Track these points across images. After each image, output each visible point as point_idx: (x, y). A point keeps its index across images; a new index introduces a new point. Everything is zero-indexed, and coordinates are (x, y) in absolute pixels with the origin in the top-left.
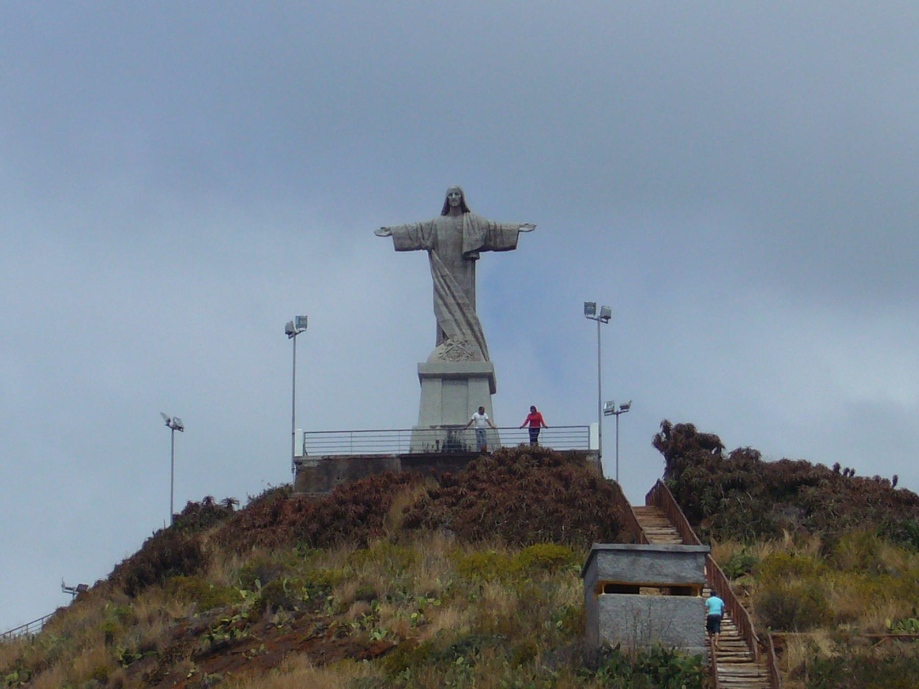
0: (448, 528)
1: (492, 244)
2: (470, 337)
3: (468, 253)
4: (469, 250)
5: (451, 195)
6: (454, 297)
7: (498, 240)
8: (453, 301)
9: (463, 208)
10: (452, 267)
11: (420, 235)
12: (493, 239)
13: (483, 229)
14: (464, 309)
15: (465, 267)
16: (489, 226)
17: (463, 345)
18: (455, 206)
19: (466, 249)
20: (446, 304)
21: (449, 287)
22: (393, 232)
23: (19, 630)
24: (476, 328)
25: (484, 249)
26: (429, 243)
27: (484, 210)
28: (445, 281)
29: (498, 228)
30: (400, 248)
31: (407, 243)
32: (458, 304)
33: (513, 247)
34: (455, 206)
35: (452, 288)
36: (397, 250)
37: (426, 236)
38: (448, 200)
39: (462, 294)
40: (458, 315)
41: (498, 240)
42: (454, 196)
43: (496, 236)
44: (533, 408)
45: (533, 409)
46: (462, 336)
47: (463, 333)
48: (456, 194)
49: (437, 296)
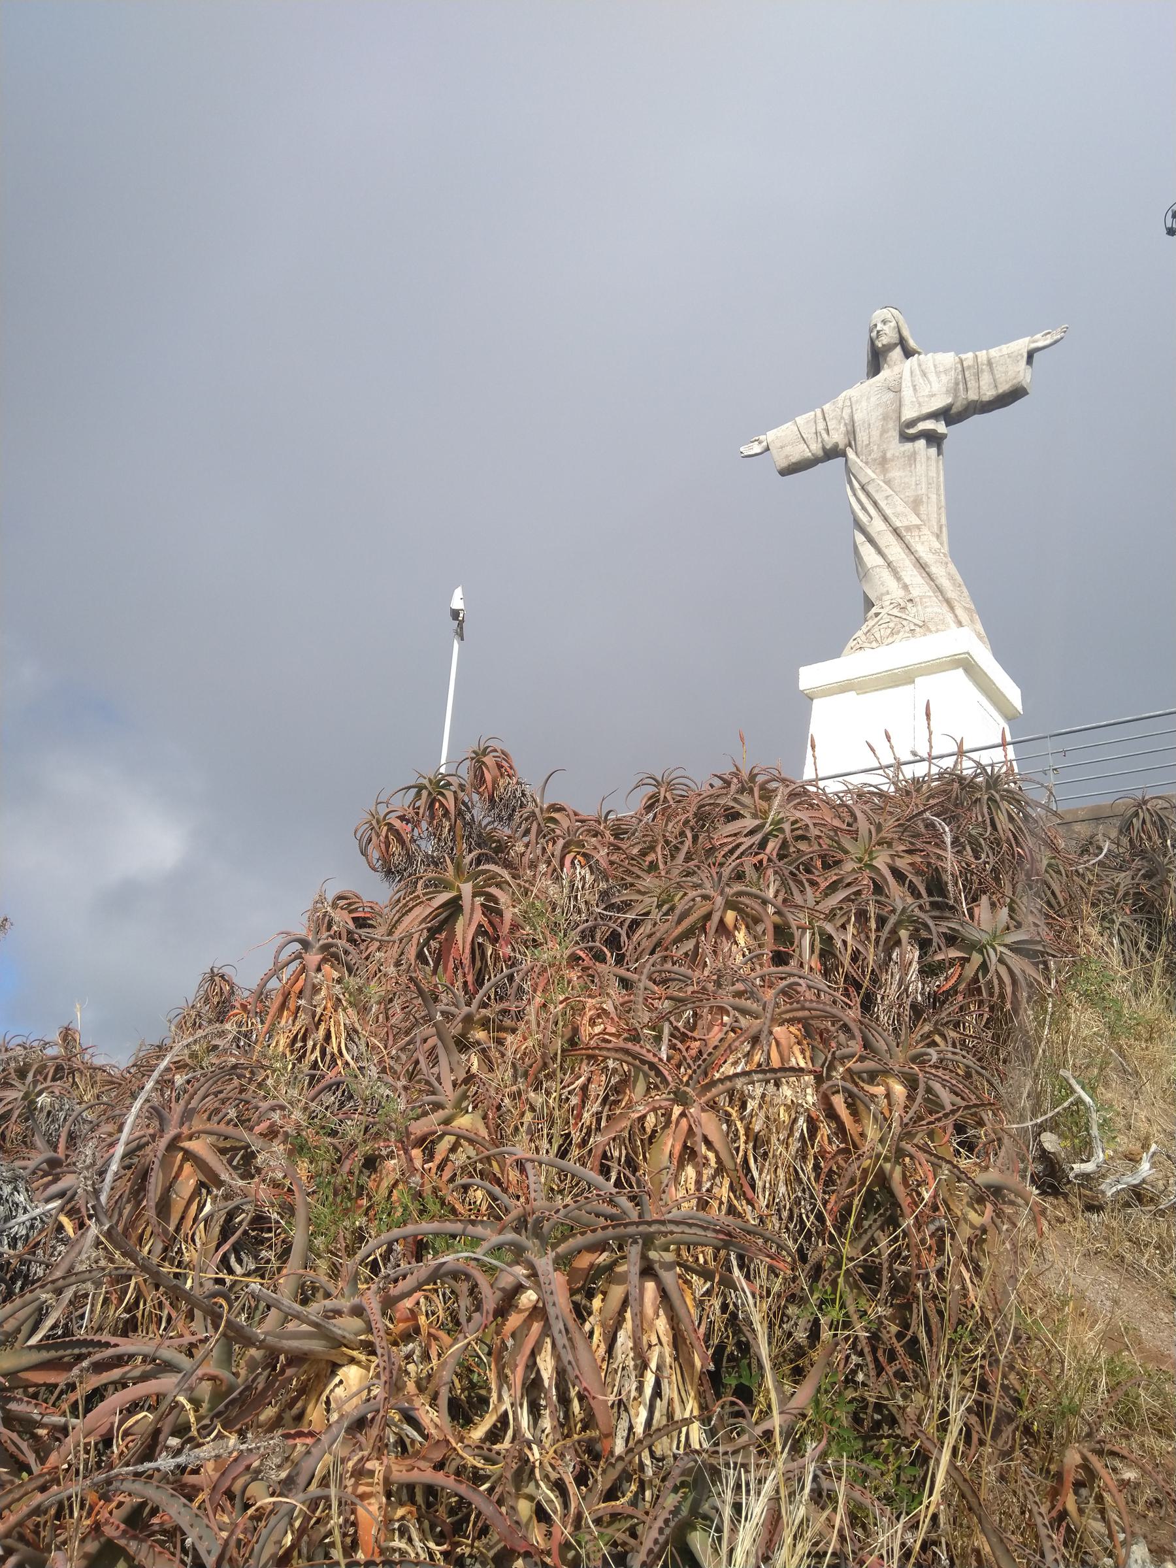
1: (973, 396)
3: (912, 423)
6: (886, 519)
11: (821, 426)
13: (946, 372)
14: (908, 538)
19: (908, 414)
32: (896, 531)
35: (882, 504)
39: (901, 507)
46: (901, 593)
47: (906, 587)
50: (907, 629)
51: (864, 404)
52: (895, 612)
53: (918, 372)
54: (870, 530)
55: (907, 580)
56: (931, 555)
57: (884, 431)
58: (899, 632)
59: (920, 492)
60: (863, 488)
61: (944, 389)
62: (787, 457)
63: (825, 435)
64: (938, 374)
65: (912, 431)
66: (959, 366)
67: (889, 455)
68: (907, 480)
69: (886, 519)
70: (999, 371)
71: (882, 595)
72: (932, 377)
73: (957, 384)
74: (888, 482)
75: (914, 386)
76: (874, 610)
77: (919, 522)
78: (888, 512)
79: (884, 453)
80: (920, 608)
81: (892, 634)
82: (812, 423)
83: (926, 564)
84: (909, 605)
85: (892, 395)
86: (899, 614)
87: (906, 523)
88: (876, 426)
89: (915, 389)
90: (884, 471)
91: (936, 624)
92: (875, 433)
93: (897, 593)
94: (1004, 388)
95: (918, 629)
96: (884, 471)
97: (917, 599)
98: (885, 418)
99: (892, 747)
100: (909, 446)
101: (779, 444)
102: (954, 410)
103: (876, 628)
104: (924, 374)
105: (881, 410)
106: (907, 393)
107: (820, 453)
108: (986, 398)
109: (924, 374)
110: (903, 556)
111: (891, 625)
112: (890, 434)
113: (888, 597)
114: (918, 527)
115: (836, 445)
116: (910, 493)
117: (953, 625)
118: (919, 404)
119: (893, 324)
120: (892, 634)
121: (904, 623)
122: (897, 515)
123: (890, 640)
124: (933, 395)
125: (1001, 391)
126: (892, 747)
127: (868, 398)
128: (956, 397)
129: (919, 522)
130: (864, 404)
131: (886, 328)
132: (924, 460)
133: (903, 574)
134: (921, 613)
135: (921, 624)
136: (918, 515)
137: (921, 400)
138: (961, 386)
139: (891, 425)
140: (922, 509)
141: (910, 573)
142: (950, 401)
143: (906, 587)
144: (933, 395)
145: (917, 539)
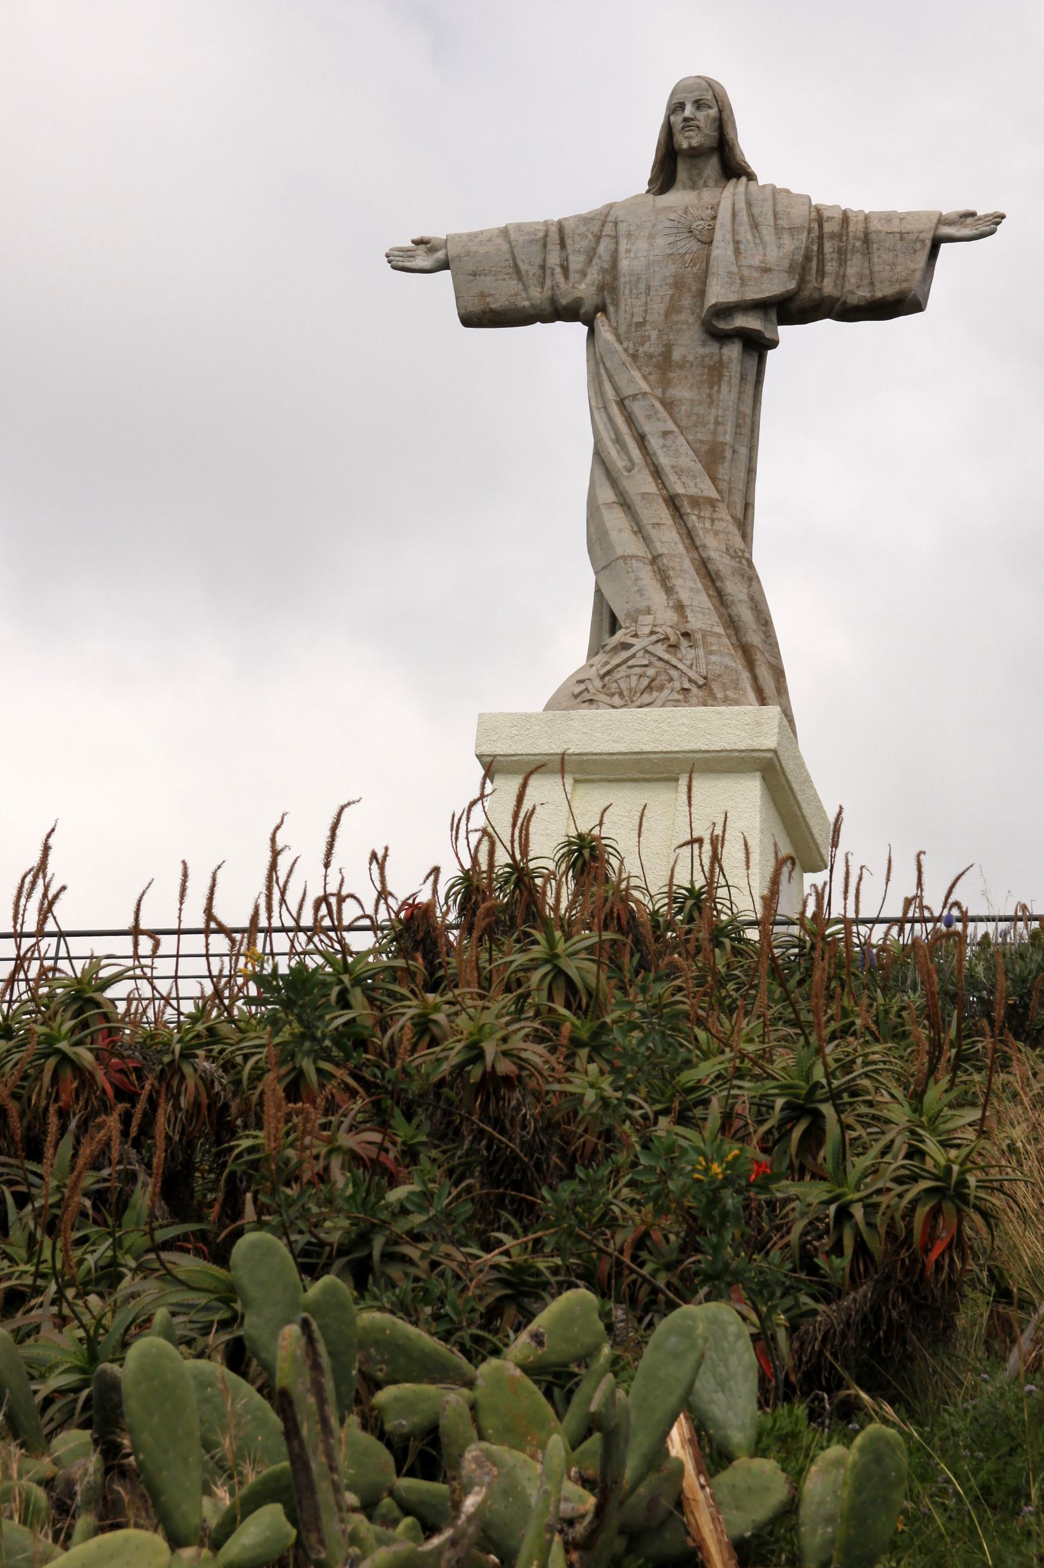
0: (696, 1274)
1: (829, 287)
2: (703, 616)
3: (725, 311)
4: (732, 298)
5: (681, 106)
6: (657, 473)
7: (859, 275)
8: (651, 487)
9: (733, 168)
10: (664, 365)
11: (554, 258)
12: (830, 267)
13: (792, 230)
14: (693, 519)
15: (716, 372)
16: (820, 220)
17: (674, 647)
18: (699, 147)
19: (718, 293)
20: (625, 504)
21: (641, 440)
22: (453, 250)
23: (990, 927)
24: (734, 588)
25: (794, 309)
26: (584, 289)
27: (807, 155)
28: (630, 420)
29: (856, 228)
30: (478, 317)
31: (504, 292)
32: (673, 502)
33: (902, 303)
34: (699, 147)
35: (655, 443)
36: (469, 320)
37: (576, 262)
38: (668, 132)
39: (687, 459)
40: (668, 539)
41: (859, 275)
42: (689, 111)
43: (842, 255)
44: (998, 218)
45: (998, 218)
46: (671, 616)
47: (680, 608)
48: (698, 104)
49: (600, 475)
50: (677, 685)
51: (642, 245)
52: (660, 650)
53: (743, 217)
54: (626, 483)
55: (684, 596)
56: (726, 559)
57: (673, 309)
58: (661, 688)
59: (720, 439)
60: (621, 403)
61: (786, 264)
62: (482, 295)
63: (559, 277)
64: (778, 229)
65: (722, 325)
66: (815, 225)
67: (676, 355)
68: (702, 410)
69: (657, 473)
70: (881, 258)
71: (638, 611)
72: (768, 233)
73: (807, 258)
74: (669, 405)
75: (737, 243)
76: (619, 636)
77: (714, 494)
78: (664, 461)
79: (668, 348)
80: (701, 652)
81: (649, 688)
82: (538, 247)
83: (717, 573)
84: (684, 643)
85: (694, 245)
86: (666, 656)
87: (693, 491)
88: (662, 294)
89: (737, 252)
90: (665, 383)
91: (725, 688)
92: (658, 307)
93: (666, 617)
94: (884, 290)
95: (694, 690)
96: (665, 383)
97: (698, 636)
98: (678, 284)
99: (180, 910)
100: (713, 348)
101: (471, 267)
102: (797, 304)
103: (623, 671)
104: (755, 225)
105: (672, 269)
106: (722, 251)
107: (547, 306)
108: (853, 300)
109: (755, 225)
110: (681, 549)
111: (651, 672)
112: (683, 317)
113: (649, 619)
114: (712, 503)
115: (578, 302)
116: (703, 435)
117: (751, 695)
118: (742, 279)
119: (713, 112)
120: (649, 688)
121: (674, 673)
122: (679, 472)
123: (646, 698)
124: (767, 270)
125: (879, 294)
126: (180, 910)
127: (651, 236)
128: (802, 281)
129: (714, 494)
130: (642, 245)
131: (701, 115)
132: (735, 381)
133: (677, 582)
134: (702, 661)
135: (701, 682)
136: (714, 479)
137: (746, 272)
138: (814, 264)
139: (687, 301)
140: (723, 471)
141: (690, 584)
142: (792, 285)
143: (680, 608)
144: (767, 270)
145: (708, 525)
